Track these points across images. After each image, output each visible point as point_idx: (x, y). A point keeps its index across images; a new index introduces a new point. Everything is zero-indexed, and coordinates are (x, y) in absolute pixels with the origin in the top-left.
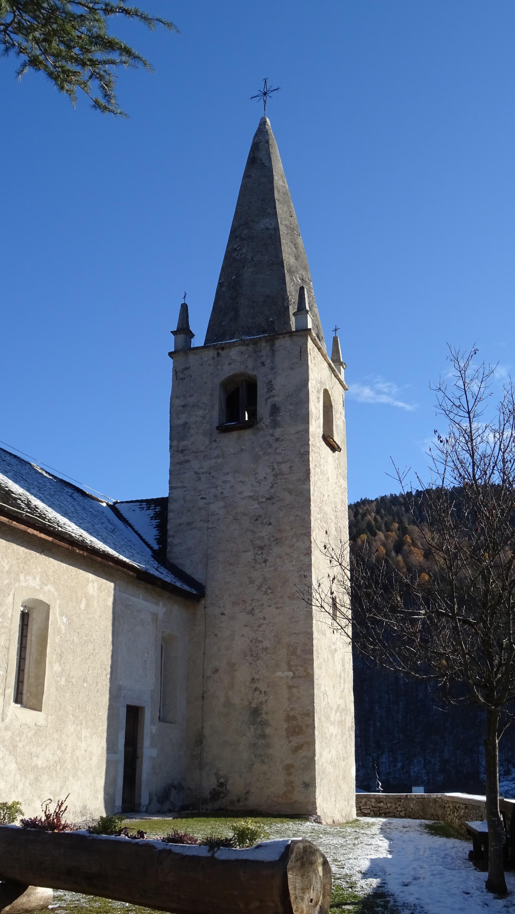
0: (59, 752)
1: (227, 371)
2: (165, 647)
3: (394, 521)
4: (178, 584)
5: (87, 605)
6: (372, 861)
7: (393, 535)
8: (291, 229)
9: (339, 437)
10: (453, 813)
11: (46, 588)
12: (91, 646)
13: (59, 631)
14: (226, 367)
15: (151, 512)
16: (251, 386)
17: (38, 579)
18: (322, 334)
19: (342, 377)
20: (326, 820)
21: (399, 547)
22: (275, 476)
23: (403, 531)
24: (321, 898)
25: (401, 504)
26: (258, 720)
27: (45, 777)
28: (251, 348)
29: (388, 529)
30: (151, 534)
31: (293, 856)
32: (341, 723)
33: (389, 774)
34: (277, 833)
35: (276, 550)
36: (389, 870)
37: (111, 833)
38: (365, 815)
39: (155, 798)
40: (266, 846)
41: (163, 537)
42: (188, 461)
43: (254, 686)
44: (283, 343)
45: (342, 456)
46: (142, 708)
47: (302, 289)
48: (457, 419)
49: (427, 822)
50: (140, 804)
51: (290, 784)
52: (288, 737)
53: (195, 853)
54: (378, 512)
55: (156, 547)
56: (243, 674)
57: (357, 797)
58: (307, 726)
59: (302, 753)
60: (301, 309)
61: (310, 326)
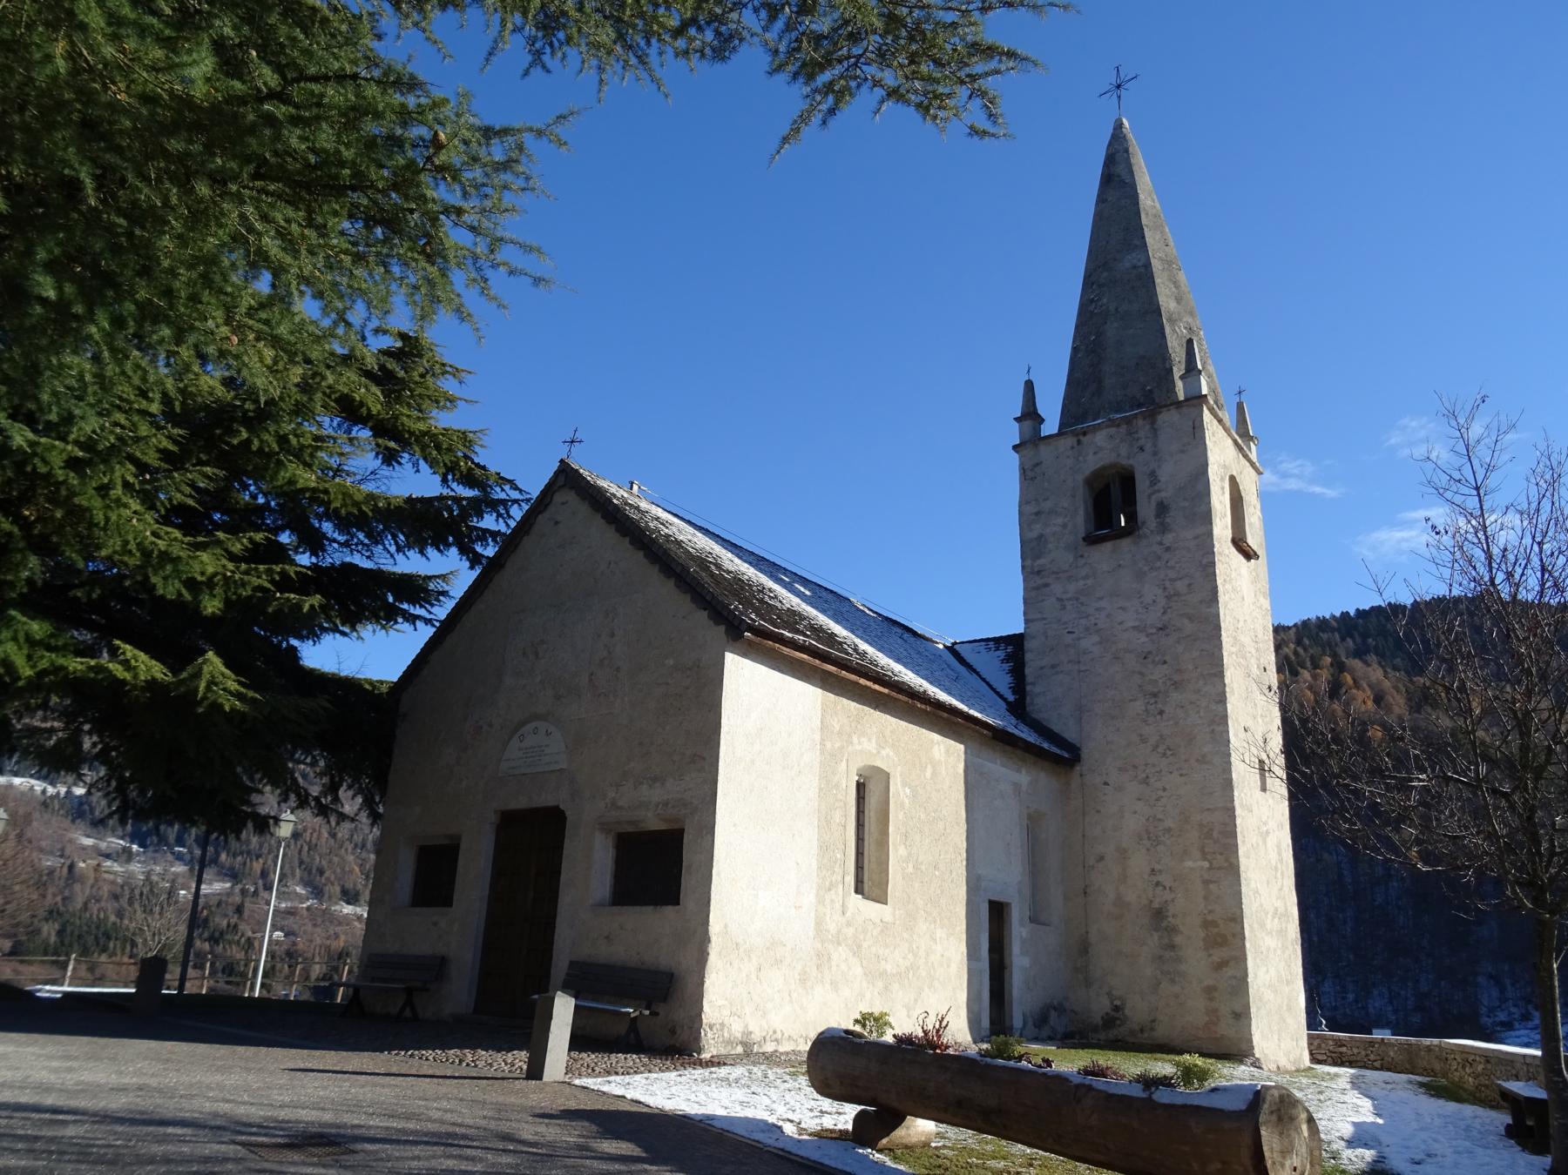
0: (910, 956)
1: (1092, 463)
2: (1033, 825)
3: (1324, 654)
4: (1045, 745)
5: (934, 774)
6: (1355, 1124)
7: (1325, 675)
8: (1168, 263)
9: (1254, 540)
10: (1464, 1067)
11: (884, 753)
12: (941, 825)
13: (902, 804)
14: (1090, 457)
15: (1001, 654)
18: (1222, 400)
19: (1253, 456)
20: (1269, 1065)
21: (1335, 690)
22: (1168, 598)
23: (1339, 667)
25: (1333, 630)
27: (896, 986)
29: (1316, 666)
30: (1003, 682)
31: (1266, 1106)
32: (1282, 933)
34: (1237, 1075)
35: (1175, 696)
36: (1385, 1139)
37: (1009, 1058)
38: (1319, 1062)
39: (1030, 1023)
40: (1225, 1089)
41: (1019, 685)
42: (1047, 585)
43: (1155, 879)
44: (1167, 418)
45: (1260, 565)
46: (1008, 905)
47: (1190, 342)
48: (1458, 499)
49: (1419, 1079)
52: (1206, 949)
53: (1124, 1092)
54: (1299, 642)
55: (1011, 698)
56: (1139, 862)
57: (1310, 1037)
58: (1234, 935)
59: (1229, 972)
60: (1191, 369)
61: (1204, 392)
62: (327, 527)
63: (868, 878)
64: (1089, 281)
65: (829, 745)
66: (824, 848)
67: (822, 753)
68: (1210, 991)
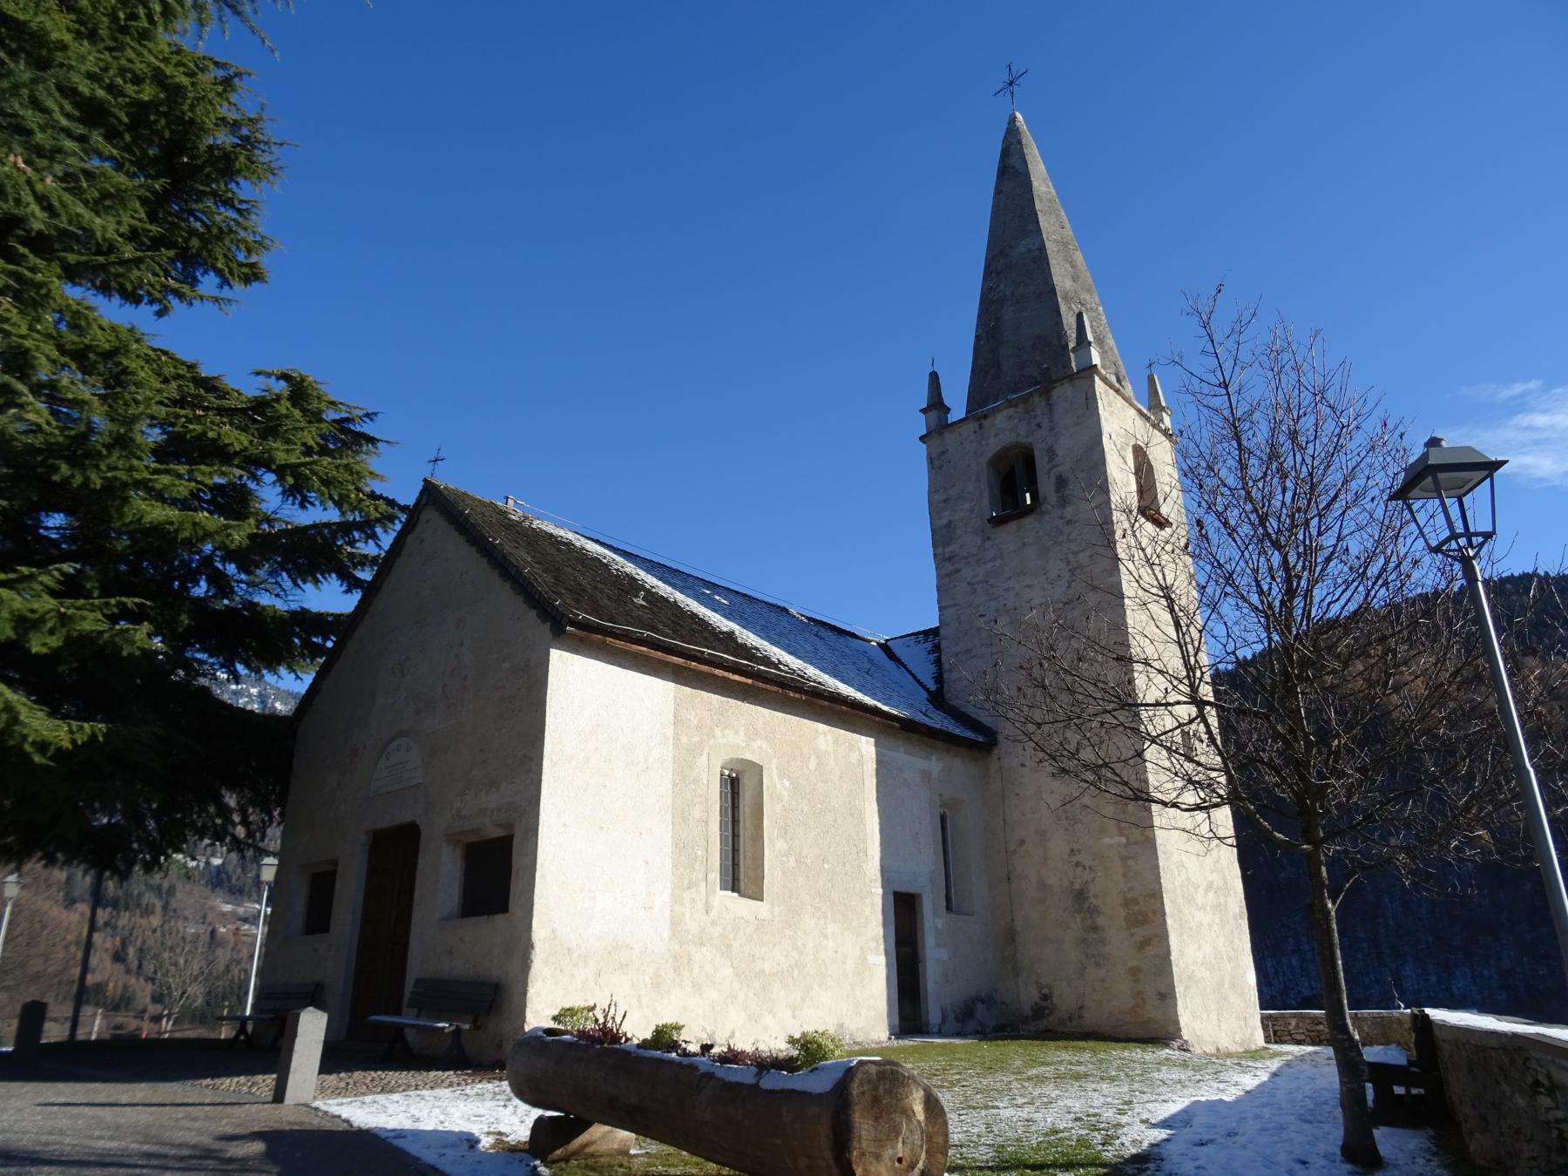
0: (795, 954)
1: (994, 445)
4: (957, 731)
5: (819, 765)
11: (755, 745)
13: (780, 799)
16: (1028, 459)
17: (742, 734)
22: (1072, 571)
24: (923, 1156)
26: (1086, 906)
28: (1021, 408)
30: (926, 673)
33: (1419, 991)
39: (951, 1016)
42: (957, 571)
43: (1074, 860)
44: (1062, 392)
46: (919, 895)
50: (927, 1024)
51: (1139, 994)
52: (1128, 928)
55: (933, 687)
56: (1058, 844)
57: (1264, 1019)
58: (1154, 912)
62: (231, 569)
63: (740, 870)
64: (989, 271)
65: (684, 739)
66: (680, 845)
67: (676, 746)
68: (1134, 972)
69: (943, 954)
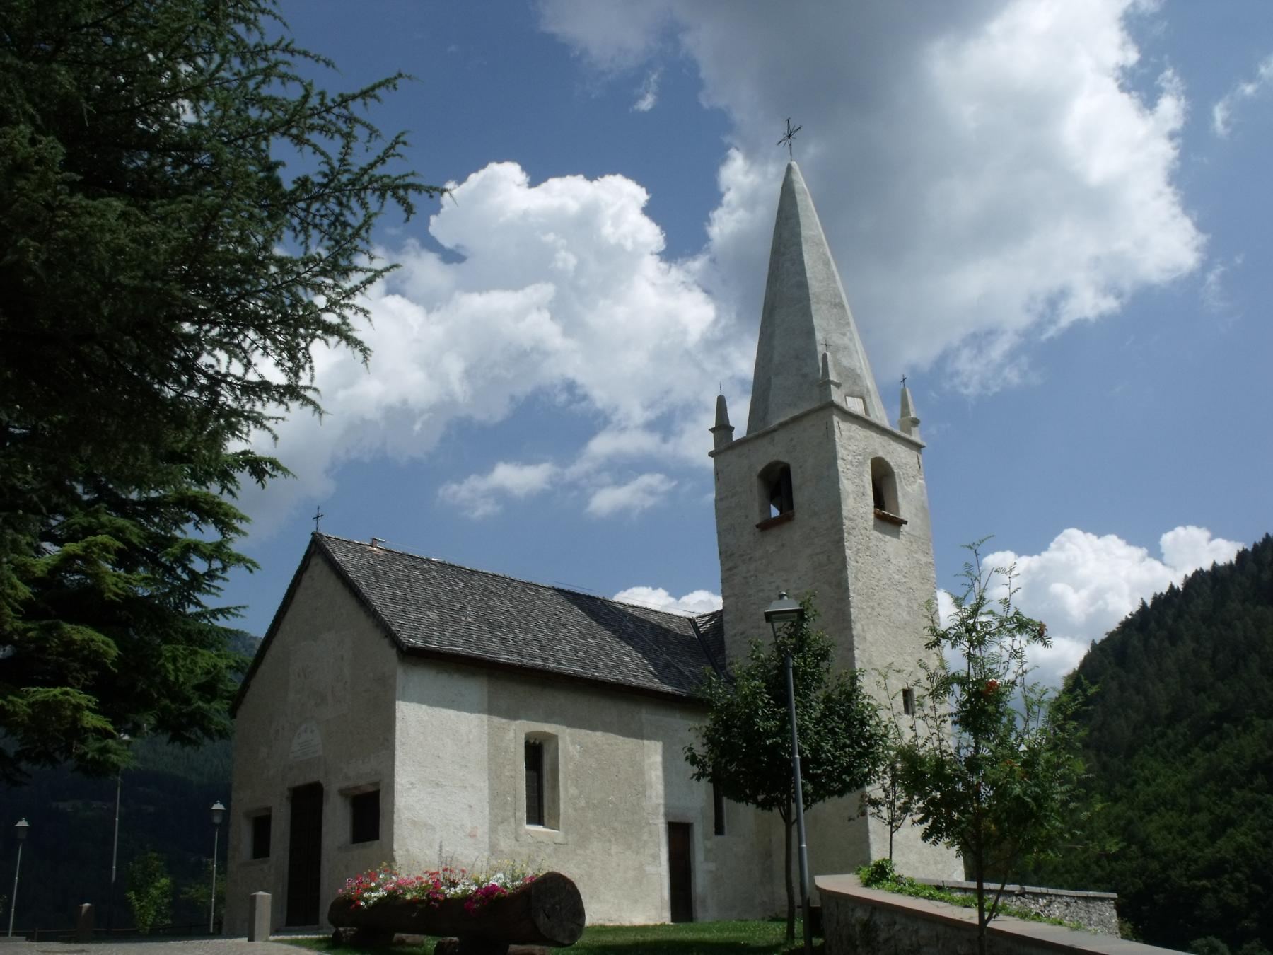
69: (712, 866)
